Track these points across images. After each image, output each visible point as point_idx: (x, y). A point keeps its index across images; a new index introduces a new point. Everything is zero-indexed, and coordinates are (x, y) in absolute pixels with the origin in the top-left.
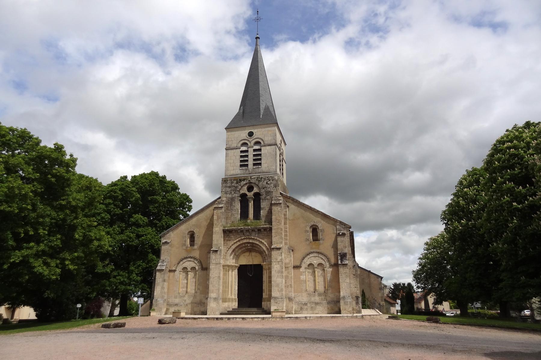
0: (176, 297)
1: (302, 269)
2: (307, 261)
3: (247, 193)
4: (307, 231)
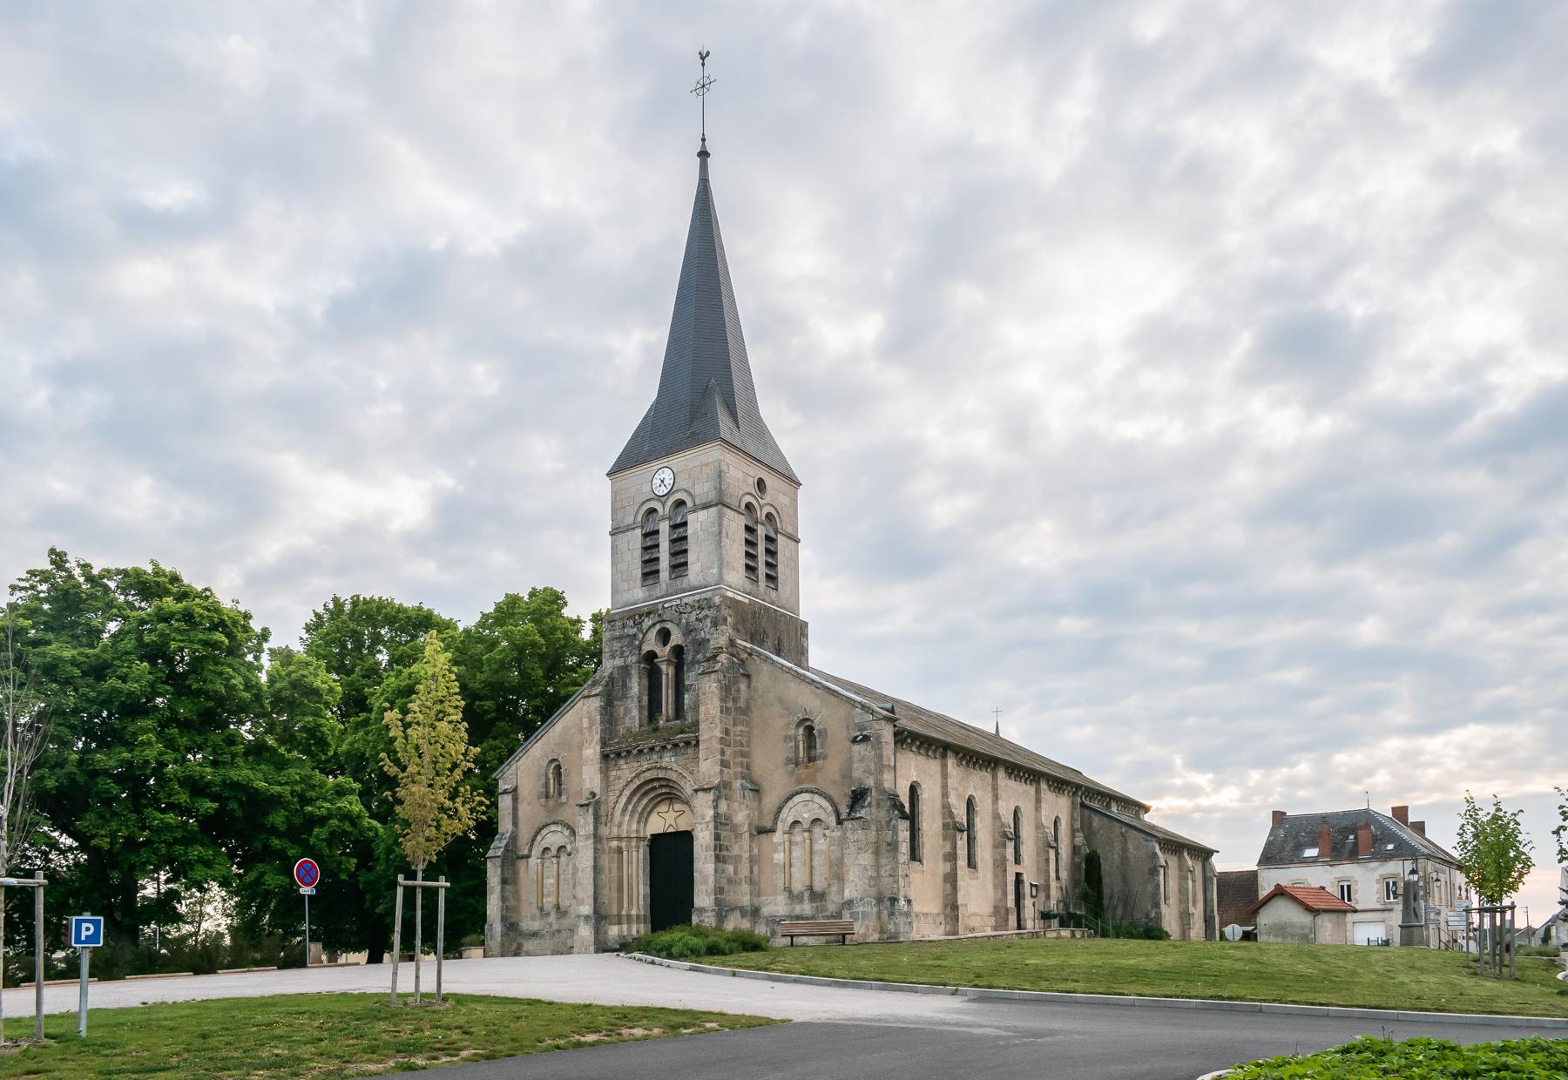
0: (533, 918)
1: (778, 837)
2: (788, 815)
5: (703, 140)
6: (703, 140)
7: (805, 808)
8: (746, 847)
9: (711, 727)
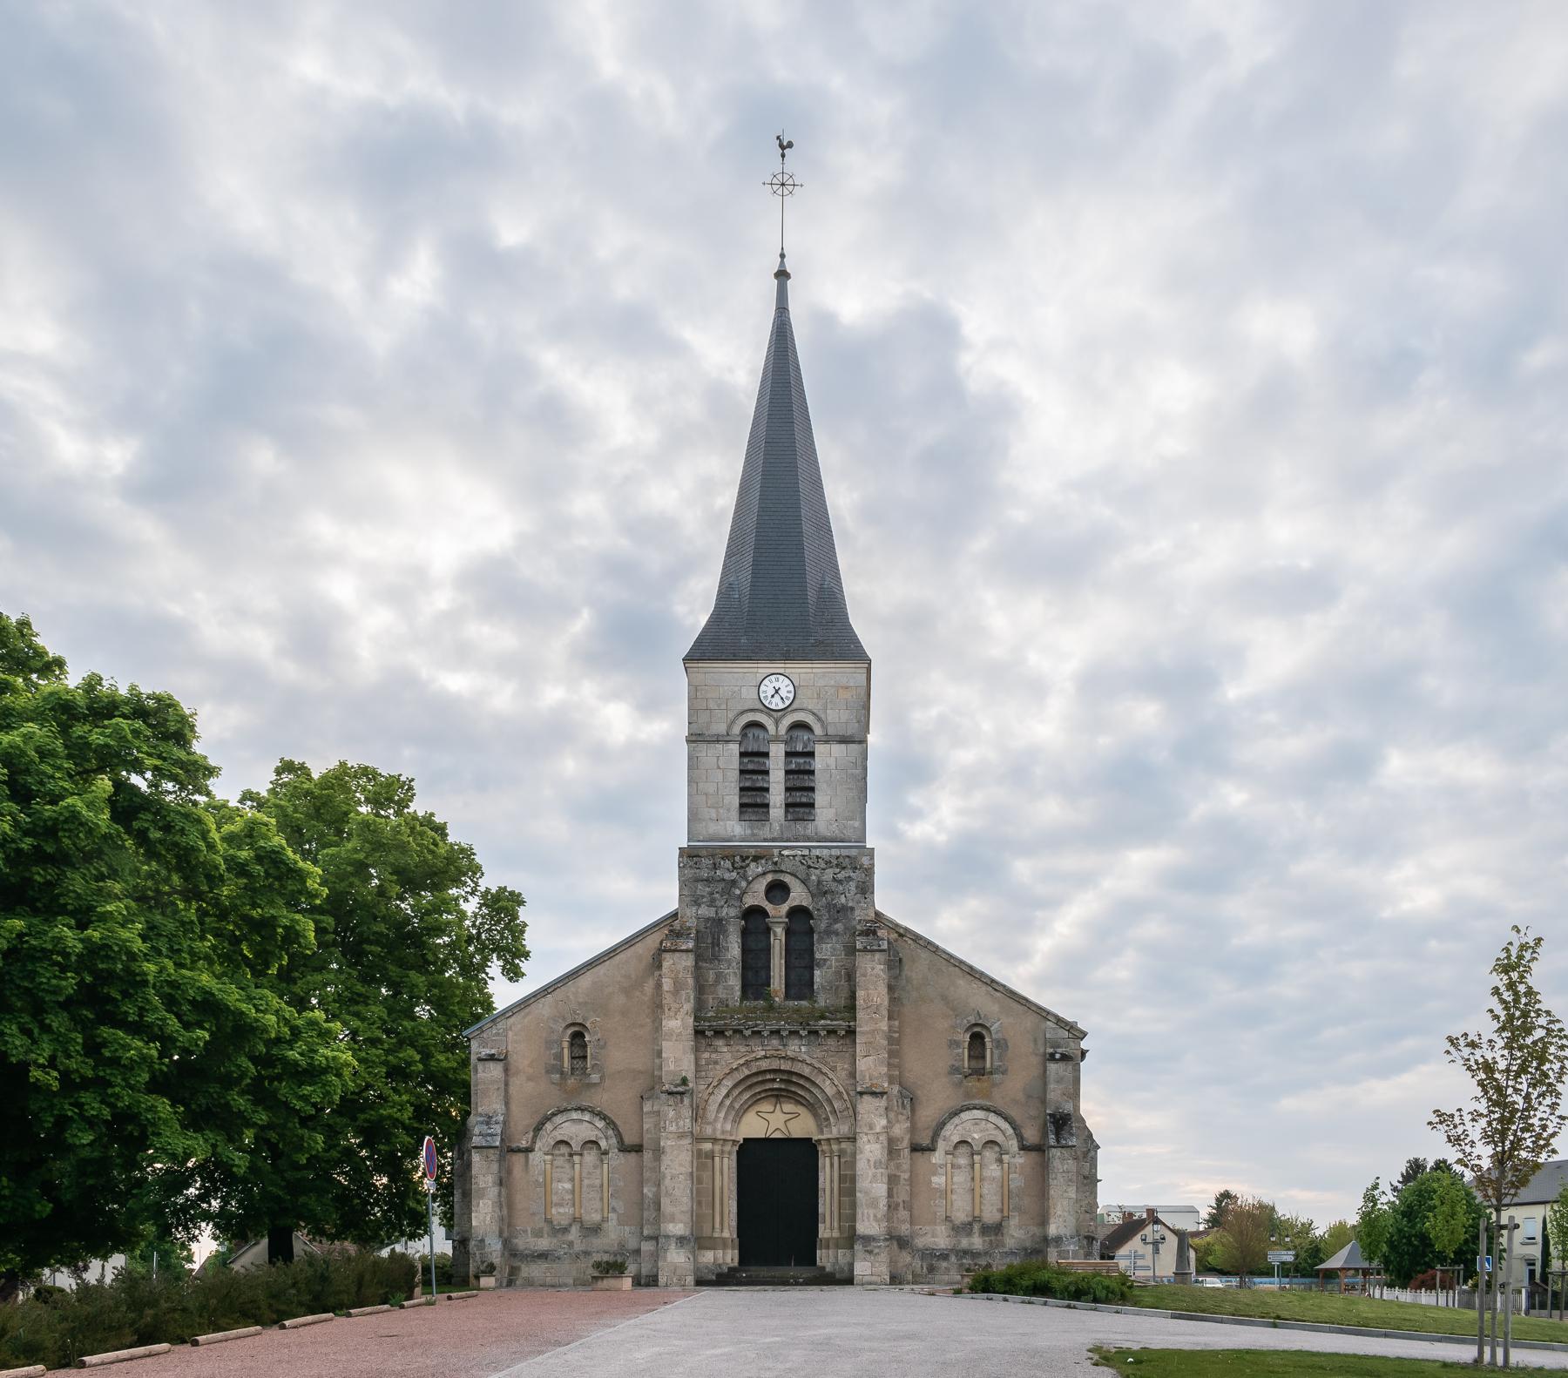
0: (538, 1234)
1: (937, 1157)
2: (952, 1133)
3: (769, 907)
4: (957, 1044)
5: (782, 256)
6: (782, 256)
7: (974, 1126)
8: (906, 1167)
9: (872, 1023)
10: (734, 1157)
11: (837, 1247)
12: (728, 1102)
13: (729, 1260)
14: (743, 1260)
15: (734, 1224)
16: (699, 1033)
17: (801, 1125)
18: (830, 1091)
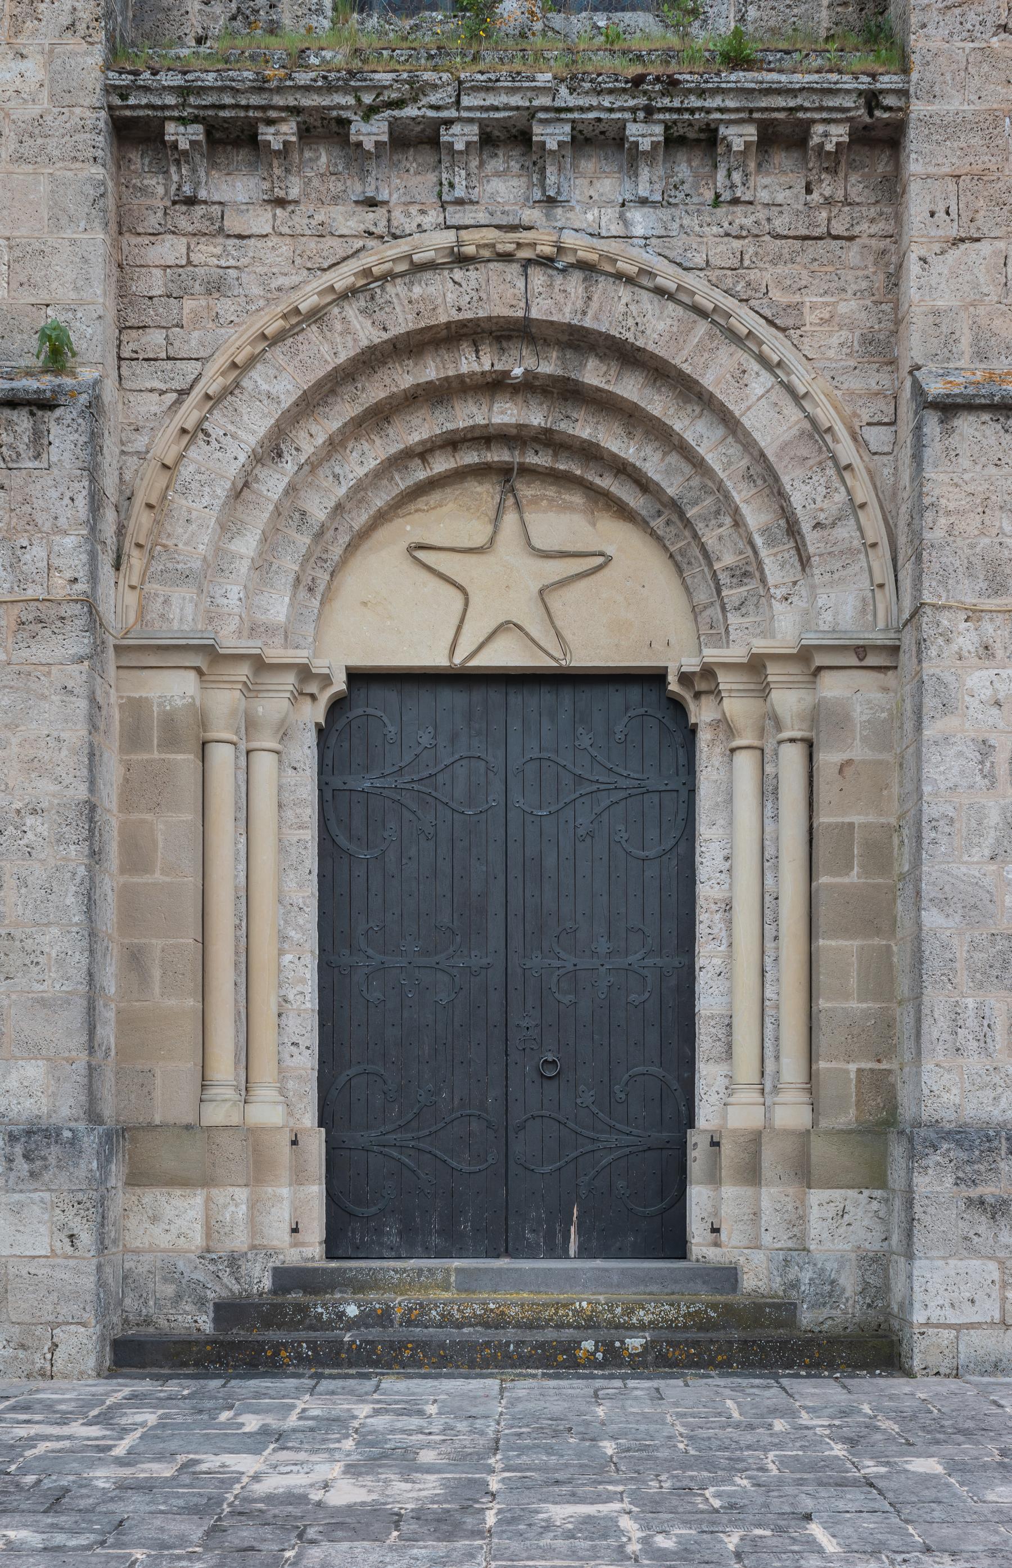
10: (305, 751)
11: (804, 1173)
12: (273, 484)
13: (278, 1235)
14: (351, 1221)
15: (305, 1062)
16: (133, 133)
17: (623, 610)
18: (770, 424)
